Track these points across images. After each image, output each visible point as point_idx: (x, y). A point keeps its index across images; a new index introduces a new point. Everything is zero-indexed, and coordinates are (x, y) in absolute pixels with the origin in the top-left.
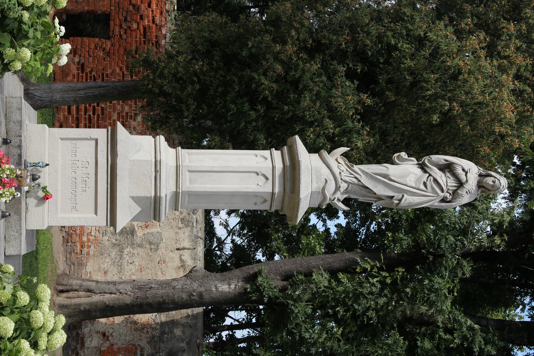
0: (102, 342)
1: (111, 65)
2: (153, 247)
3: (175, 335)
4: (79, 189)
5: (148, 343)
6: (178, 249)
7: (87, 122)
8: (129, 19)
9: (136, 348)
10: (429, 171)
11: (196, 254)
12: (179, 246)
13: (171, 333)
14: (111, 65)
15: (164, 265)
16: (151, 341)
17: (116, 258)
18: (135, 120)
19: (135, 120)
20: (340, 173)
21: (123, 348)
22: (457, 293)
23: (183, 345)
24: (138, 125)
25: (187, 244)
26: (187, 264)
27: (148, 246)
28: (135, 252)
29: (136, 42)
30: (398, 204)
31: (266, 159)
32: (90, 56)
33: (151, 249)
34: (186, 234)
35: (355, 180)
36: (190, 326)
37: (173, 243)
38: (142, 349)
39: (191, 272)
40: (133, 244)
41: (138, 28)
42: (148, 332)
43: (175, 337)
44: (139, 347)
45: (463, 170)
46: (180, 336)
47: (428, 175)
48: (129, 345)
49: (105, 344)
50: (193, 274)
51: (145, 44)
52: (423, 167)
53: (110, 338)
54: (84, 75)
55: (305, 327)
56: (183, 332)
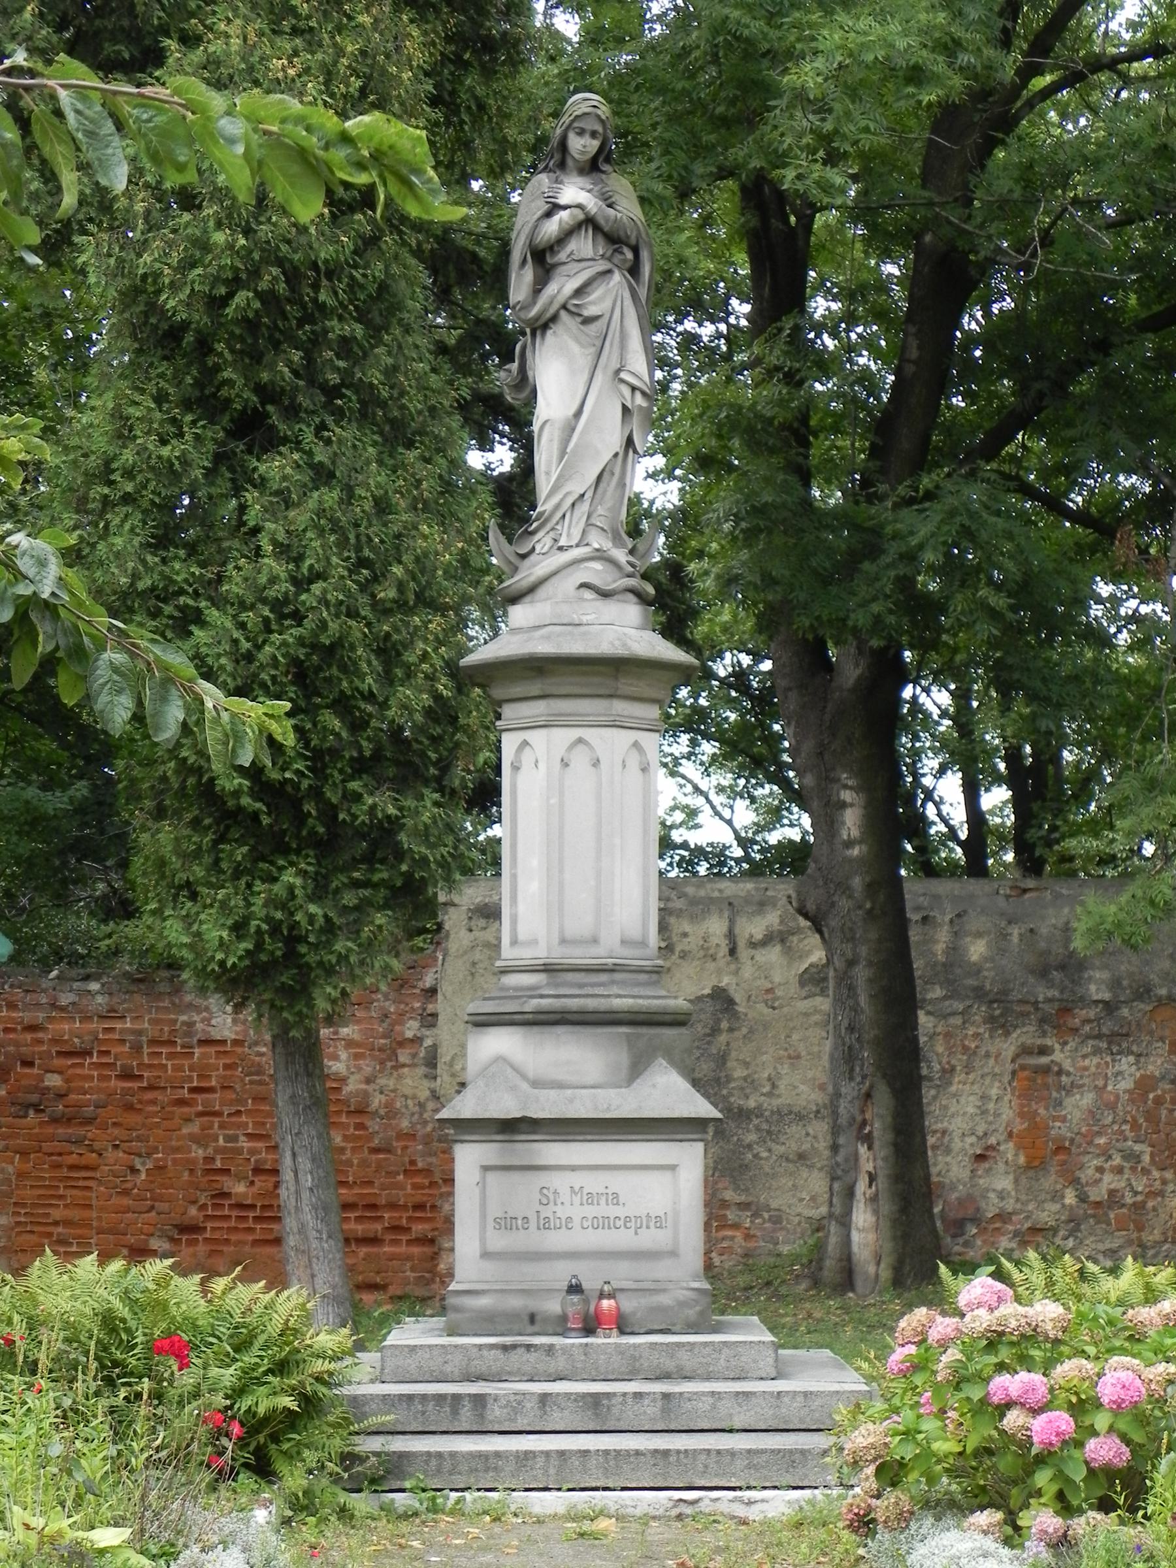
0: (1001, 1166)
1: (177, 1150)
2: (724, 1025)
3: (986, 959)
4: (613, 1211)
5: (1007, 1034)
6: (733, 952)
7: (352, 1215)
8: (34, 1098)
9: (1023, 1068)
10: (552, 311)
11: (747, 900)
12: (724, 950)
13: (979, 971)
14: (177, 1150)
15: (779, 993)
16: (1003, 1026)
17: (758, 1129)
18: (343, 1080)
19: (343, 1080)
20: (561, 549)
21: (1022, 1106)
22: (886, 255)
23: (1015, 932)
24: (359, 1069)
25: (716, 926)
26: (776, 927)
27: (723, 1038)
28: (739, 1073)
29: (102, 1078)
30: (644, 393)
31: (525, 743)
32: (152, 1208)
33: (731, 1030)
34: (686, 927)
35: (584, 507)
36: (959, 916)
37: (711, 966)
38: (1025, 1051)
39: (806, 916)
40: (717, 1080)
41: (60, 1073)
42: (976, 1035)
43: (992, 960)
44: (1020, 1061)
45: (548, 214)
46: (989, 945)
47: (563, 313)
48: (1013, 1089)
49: (1010, 1156)
50: (811, 907)
51: (108, 1053)
52: (542, 326)
53: (992, 1140)
54: (209, 1225)
55: (936, 79)
56: (979, 935)
